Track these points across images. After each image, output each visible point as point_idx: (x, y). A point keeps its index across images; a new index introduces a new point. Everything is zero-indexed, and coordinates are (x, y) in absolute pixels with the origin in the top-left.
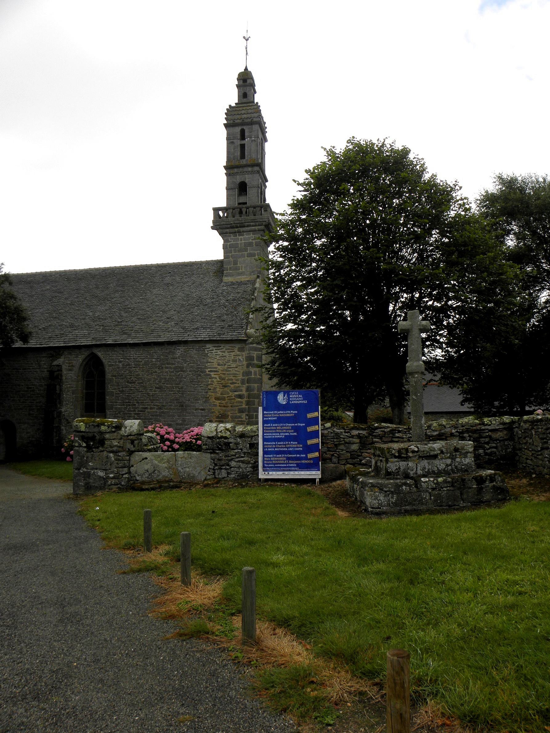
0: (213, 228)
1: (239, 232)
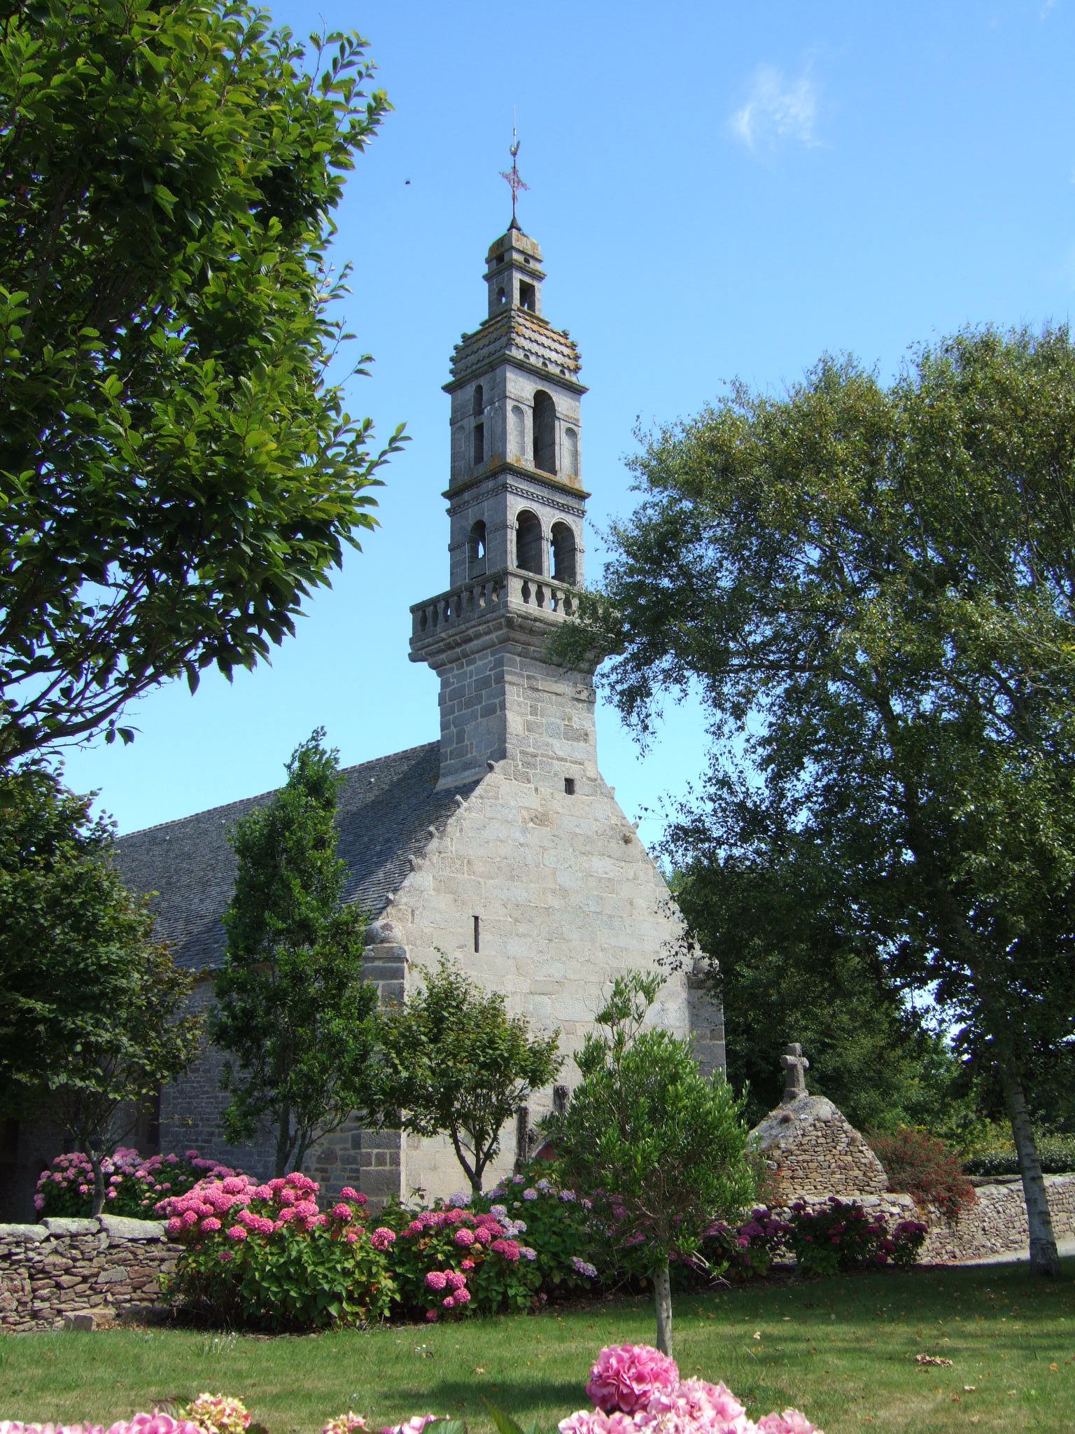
0: (414, 658)
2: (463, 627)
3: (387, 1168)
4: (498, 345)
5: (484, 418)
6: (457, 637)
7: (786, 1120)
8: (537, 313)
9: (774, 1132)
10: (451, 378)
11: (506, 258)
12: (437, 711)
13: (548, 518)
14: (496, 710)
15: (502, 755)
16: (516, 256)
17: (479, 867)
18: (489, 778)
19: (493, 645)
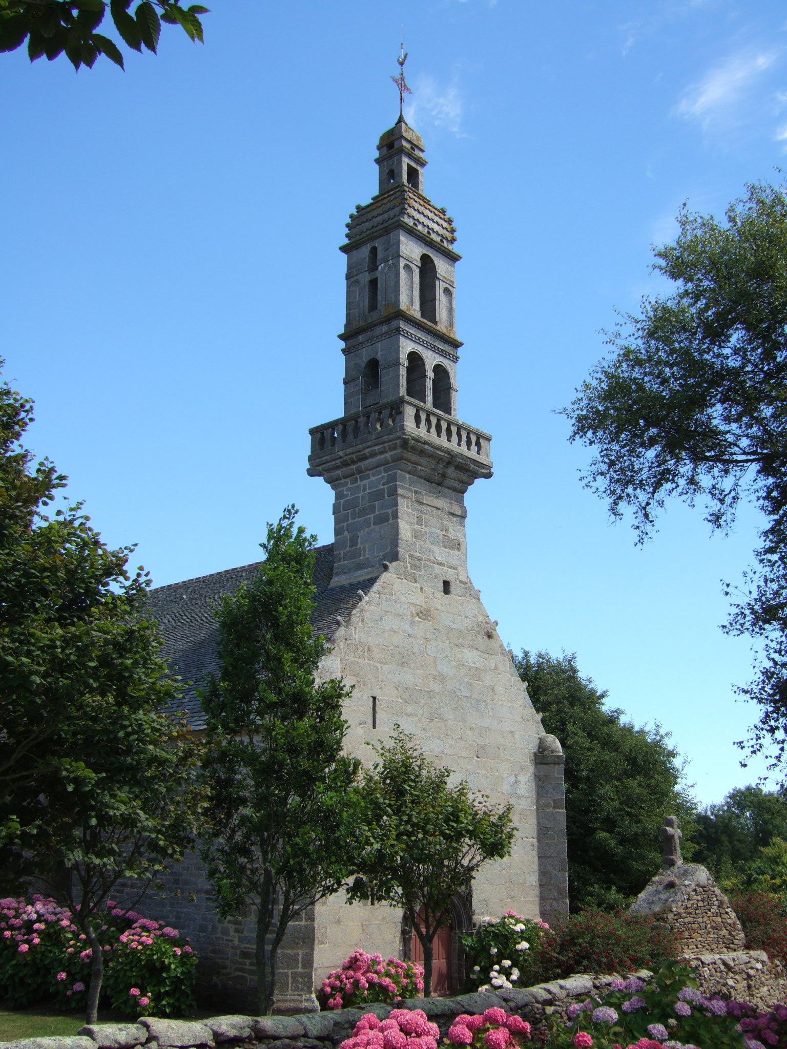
0: (311, 473)
1: (360, 471)
2: (360, 447)
3: (303, 923)
4: (391, 214)
5: (378, 274)
6: (354, 456)
7: (671, 885)
8: (420, 192)
9: (663, 897)
10: (346, 241)
11: (396, 145)
12: (331, 519)
13: (431, 360)
14: (390, 518)
15: (395, 557)
16: (404, 143)
17: (377, 654)
18: (385, 576)
19: (387, 463)
